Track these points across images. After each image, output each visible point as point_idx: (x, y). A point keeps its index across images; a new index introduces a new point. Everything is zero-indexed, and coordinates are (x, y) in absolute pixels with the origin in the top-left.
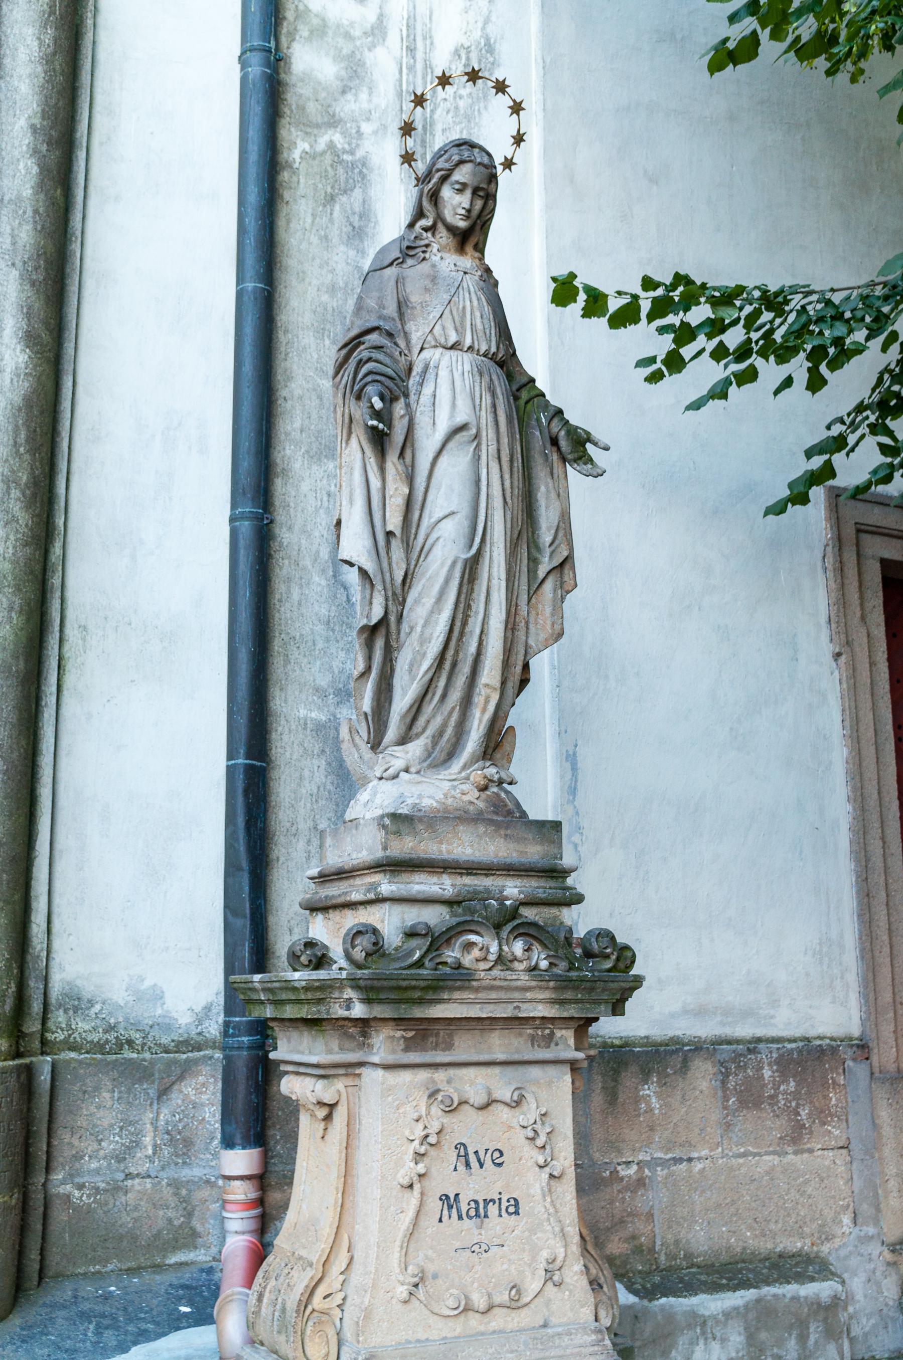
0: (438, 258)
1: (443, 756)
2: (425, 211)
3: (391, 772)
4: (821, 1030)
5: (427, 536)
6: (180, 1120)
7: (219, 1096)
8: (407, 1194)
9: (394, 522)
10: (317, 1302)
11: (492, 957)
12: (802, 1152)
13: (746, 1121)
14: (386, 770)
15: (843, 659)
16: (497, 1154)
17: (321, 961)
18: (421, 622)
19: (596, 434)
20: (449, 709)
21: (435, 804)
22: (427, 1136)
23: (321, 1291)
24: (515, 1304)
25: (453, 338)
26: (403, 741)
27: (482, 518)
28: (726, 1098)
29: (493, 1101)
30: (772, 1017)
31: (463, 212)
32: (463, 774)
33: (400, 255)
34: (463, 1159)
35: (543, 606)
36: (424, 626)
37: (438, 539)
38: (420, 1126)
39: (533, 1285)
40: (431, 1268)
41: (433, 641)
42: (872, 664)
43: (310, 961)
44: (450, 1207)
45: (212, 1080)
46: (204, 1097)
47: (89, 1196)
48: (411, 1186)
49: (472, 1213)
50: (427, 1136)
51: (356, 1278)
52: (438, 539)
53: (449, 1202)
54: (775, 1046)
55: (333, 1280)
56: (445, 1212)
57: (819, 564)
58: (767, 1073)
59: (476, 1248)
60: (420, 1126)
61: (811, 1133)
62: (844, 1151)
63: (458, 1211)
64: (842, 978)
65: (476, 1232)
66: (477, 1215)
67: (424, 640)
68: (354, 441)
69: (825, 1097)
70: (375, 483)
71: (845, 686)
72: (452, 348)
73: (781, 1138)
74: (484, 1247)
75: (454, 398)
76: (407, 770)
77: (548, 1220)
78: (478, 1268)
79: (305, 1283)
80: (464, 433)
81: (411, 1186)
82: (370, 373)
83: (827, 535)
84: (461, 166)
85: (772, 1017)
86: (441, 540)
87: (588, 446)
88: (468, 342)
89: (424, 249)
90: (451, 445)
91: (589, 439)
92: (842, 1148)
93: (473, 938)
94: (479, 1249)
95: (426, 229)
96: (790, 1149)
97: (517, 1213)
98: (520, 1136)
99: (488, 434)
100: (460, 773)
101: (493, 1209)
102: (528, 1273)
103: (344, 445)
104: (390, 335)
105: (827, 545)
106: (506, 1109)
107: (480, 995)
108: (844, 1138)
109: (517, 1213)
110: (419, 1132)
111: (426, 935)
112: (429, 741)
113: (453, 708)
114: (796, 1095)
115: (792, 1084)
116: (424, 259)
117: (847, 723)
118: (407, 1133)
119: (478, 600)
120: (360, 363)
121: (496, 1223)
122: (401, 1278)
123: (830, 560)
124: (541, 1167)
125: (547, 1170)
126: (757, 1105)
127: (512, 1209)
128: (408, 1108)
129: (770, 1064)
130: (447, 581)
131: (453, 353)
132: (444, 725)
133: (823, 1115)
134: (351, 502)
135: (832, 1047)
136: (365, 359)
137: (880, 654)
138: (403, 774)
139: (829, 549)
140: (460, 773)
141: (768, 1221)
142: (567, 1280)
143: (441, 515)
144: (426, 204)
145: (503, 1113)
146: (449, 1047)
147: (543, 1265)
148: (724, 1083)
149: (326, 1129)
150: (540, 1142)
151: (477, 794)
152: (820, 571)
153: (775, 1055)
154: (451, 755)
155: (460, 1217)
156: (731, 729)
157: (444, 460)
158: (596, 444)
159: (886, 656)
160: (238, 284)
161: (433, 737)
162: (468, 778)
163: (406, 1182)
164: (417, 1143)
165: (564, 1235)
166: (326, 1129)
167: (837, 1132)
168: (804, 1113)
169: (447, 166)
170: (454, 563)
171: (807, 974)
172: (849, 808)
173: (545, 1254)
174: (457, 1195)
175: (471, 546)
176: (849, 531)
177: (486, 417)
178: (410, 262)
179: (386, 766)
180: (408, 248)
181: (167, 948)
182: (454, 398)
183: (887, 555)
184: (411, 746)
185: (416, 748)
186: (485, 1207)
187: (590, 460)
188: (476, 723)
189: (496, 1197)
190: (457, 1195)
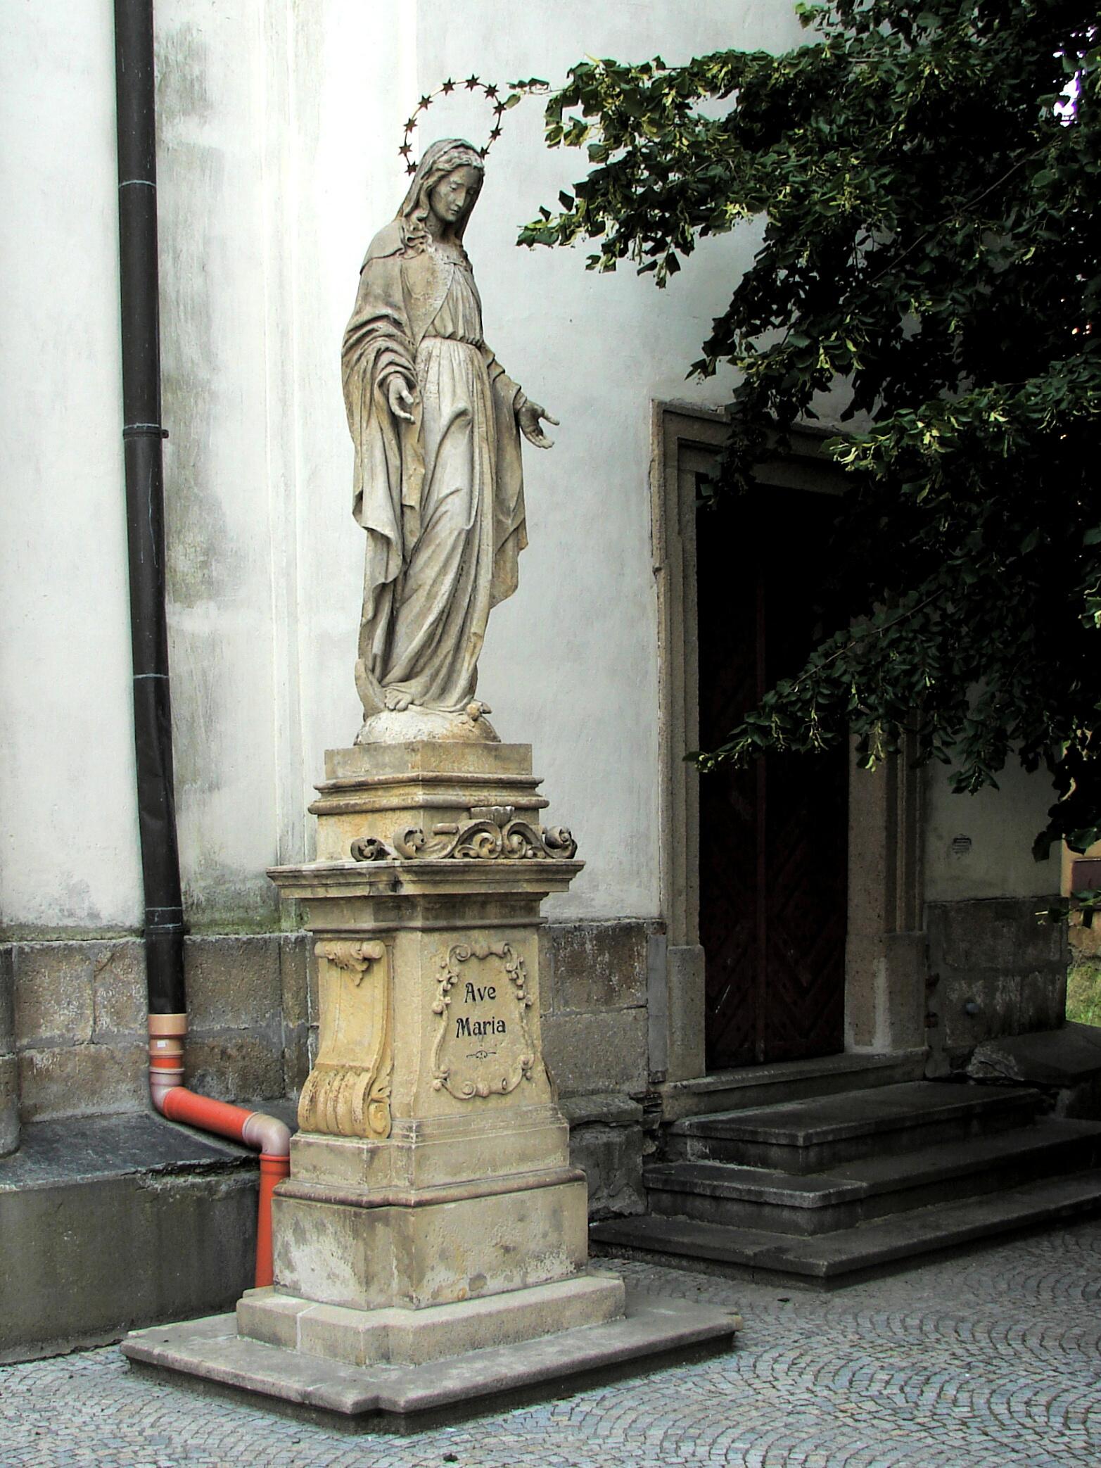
0: (433, 249)
1: (439, 691)
2: (421, 203)
3: (402, 704)
4: (628, 912)
5: (437, 509)
6: (113, 996)
7: (143, 976)
8: (438, 1018)
9: (412, 499)
10: (375, 1094)
11: (499, 849)
12: (611, 1011)
13: (571, 987)
14: (398, 703)
15: (662, 573)
16: (491, 991)
17: (381, 854)
18: (430, 582)
19: (548, 413)
20: (444, 653)
21: (445, 732)
22: (450, 978)
23: (376, 1087)
24: (503, 1093)
25: (450, 330)
26: (406, 678)
27: (476, 493)
28: (557, 969)
29: (492, 954)
30: (593, 899)
31: (456, 208)
32: (458, 707)
33: (402, 246)
34: (470, 995)
35: (505, 562)
36: (432, 586)
37: (446, 512)
38: (446, 971)
39: (515, 1079)
40: (453, 1068)
41: (439, 598)
42: (685, 577)
43: (372, 854)
44: (463, 1027)
45: (135, 962)
46: (131, 976)
47: (48, 1059)
48: (441, 1014)
49: (477, 1031)
50: (450, 978)
51: (397, 1078)
52: (446, 512)
53: (463, 1024)
54: (595, 924)
55: (383, 1081)
56: (460, 1031)
57: (646, 479)
58: (588, 946)
59: (479, 1055)
60: (446, 971)
61: (620, 996)
62: (643, 1009)
63: (469, 1029)
64: (647, 865)
65: (479, 1044)
66: (480, 1033)
67: (431, 596)
68: (374, 422)
69: (632, 966)
70: (394, 461)
71: (662, 599)
72: (449, 337)
73: (597, 1000)
74: (484, 1054)
75: (454, 386)
76: (412, 703)
77: (524, 1036)
78: (481, 1068)
79: (366, 1081)
80: (462, 418)
81: (441, 1014)
82: (391, 363)
83: (653, 450)
84: (460, 169)
85: (593, 899)
86: (449, 514)
87: (541, 420)
88: (461, 333)
89: (421, 240)
90: (453, 429)
91: (543, 415)
92: (642, 1007)
93: (485, 835)
94: (481, 1055)
95: (420, 220)
96: (603, 1009)
97: (504, 1031)
98: (505, 978)
99: (479, 418)
100: (455, 705)
101: (489, 1028)
102: (511, 1070)
103: (364, 425)
104: (397, 324)
105: (653, 461)
106: (497, 960)
107: (489, 877)
108: (644, 999)
109: (504, 1031)
110: (445, 976)
111: (454, 834)
112: (428, 679)
113: (448, 652)
114: (610, 965)
115: (607, 955)
116: (423, 251)
117: (663, 636)
118: (438, 976)
119: (470, 562)
120: (379, 353)
121: (491, 1038)
122: (437, 1074)
123: (655, 474)
124: (519, 999)
125: (525, 1001)
126: (580, 973)
127: (500, 1029)
128: (437, 959)
129: (591, 941)
130: (454, 548)
131: (449, 342)
132: (441, 666)
133: (629, 980)
134: (372, 478)
135: (638, 924)
136: (383, 349)
137: (691, 568)
138: (410, 706)
139: (656, 465)
140: (455, 705)
141: (584, 1066)
142: (535, 1076)
143: (448, 491)
144: (423, 198)
145: (495, 962)
146: (462, 918)
147: (520, 1066)
148: (555, 955)
149: (362, 979)
150: (520, 982)
151: (472, 723)
152: (646, 486)
153: (595, 932)
154: (444, 691)
155: (469, 1034)
156: (568, 642)
157: (448, 444)
158: (547, 418)
159: (695, 570)
160: (120, 181)
161: (432, 675)
162: (463, 709)
163: (439, 1009)
164: (445, 982)
165: (534, 1046)
166: (362, 979)
167: (638, 994)
168: (615, 979)
169: (447, 167)
170: (459, 534)
171: (621, 863)
172: (660, 714)
173: (522, 1058)
174: (467, 1019)
175: (469, 520)
176: (674, 447)
177: (478, 404)
178: (411, 252)
179: (396, 700)
180: (409, 239)
181: (89, 847)
182: (454, 386)
183: (701, 471)
184: (413, 682)
185: (415, 686)
186: (484, 1028)
187: (541, 432)
188: (466, 664)
189: (491, 1021)
190: (467, 1019)
